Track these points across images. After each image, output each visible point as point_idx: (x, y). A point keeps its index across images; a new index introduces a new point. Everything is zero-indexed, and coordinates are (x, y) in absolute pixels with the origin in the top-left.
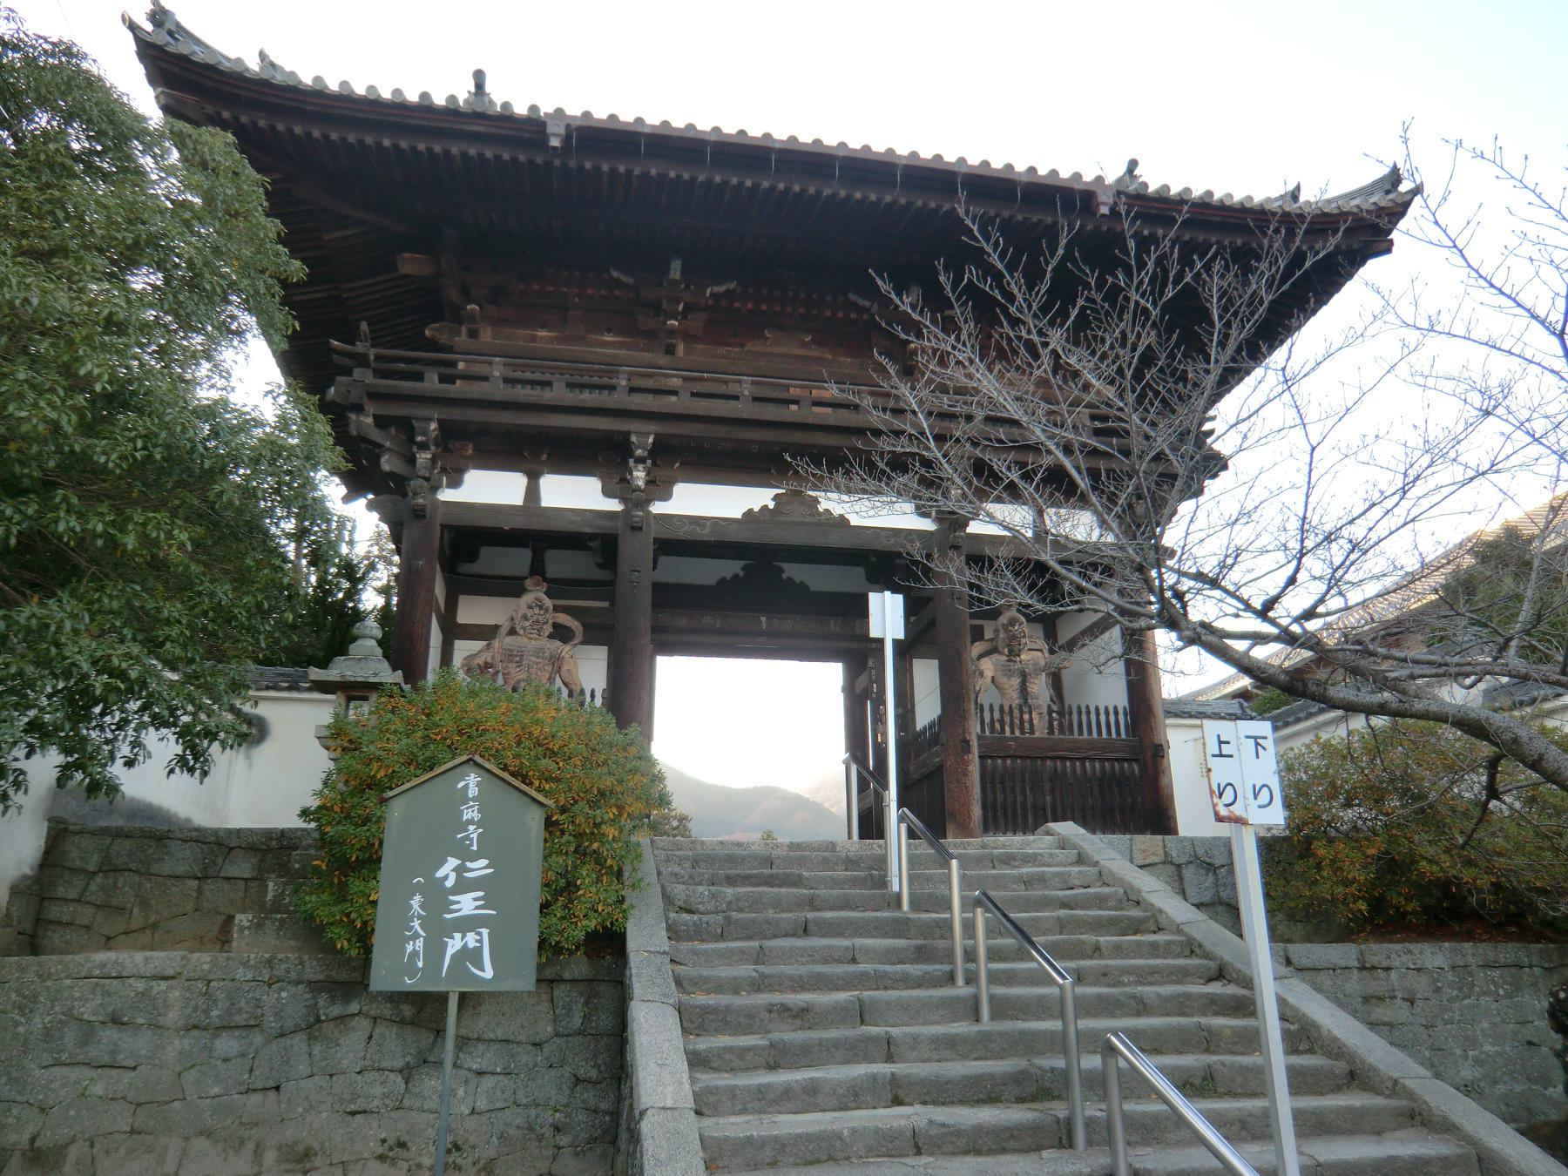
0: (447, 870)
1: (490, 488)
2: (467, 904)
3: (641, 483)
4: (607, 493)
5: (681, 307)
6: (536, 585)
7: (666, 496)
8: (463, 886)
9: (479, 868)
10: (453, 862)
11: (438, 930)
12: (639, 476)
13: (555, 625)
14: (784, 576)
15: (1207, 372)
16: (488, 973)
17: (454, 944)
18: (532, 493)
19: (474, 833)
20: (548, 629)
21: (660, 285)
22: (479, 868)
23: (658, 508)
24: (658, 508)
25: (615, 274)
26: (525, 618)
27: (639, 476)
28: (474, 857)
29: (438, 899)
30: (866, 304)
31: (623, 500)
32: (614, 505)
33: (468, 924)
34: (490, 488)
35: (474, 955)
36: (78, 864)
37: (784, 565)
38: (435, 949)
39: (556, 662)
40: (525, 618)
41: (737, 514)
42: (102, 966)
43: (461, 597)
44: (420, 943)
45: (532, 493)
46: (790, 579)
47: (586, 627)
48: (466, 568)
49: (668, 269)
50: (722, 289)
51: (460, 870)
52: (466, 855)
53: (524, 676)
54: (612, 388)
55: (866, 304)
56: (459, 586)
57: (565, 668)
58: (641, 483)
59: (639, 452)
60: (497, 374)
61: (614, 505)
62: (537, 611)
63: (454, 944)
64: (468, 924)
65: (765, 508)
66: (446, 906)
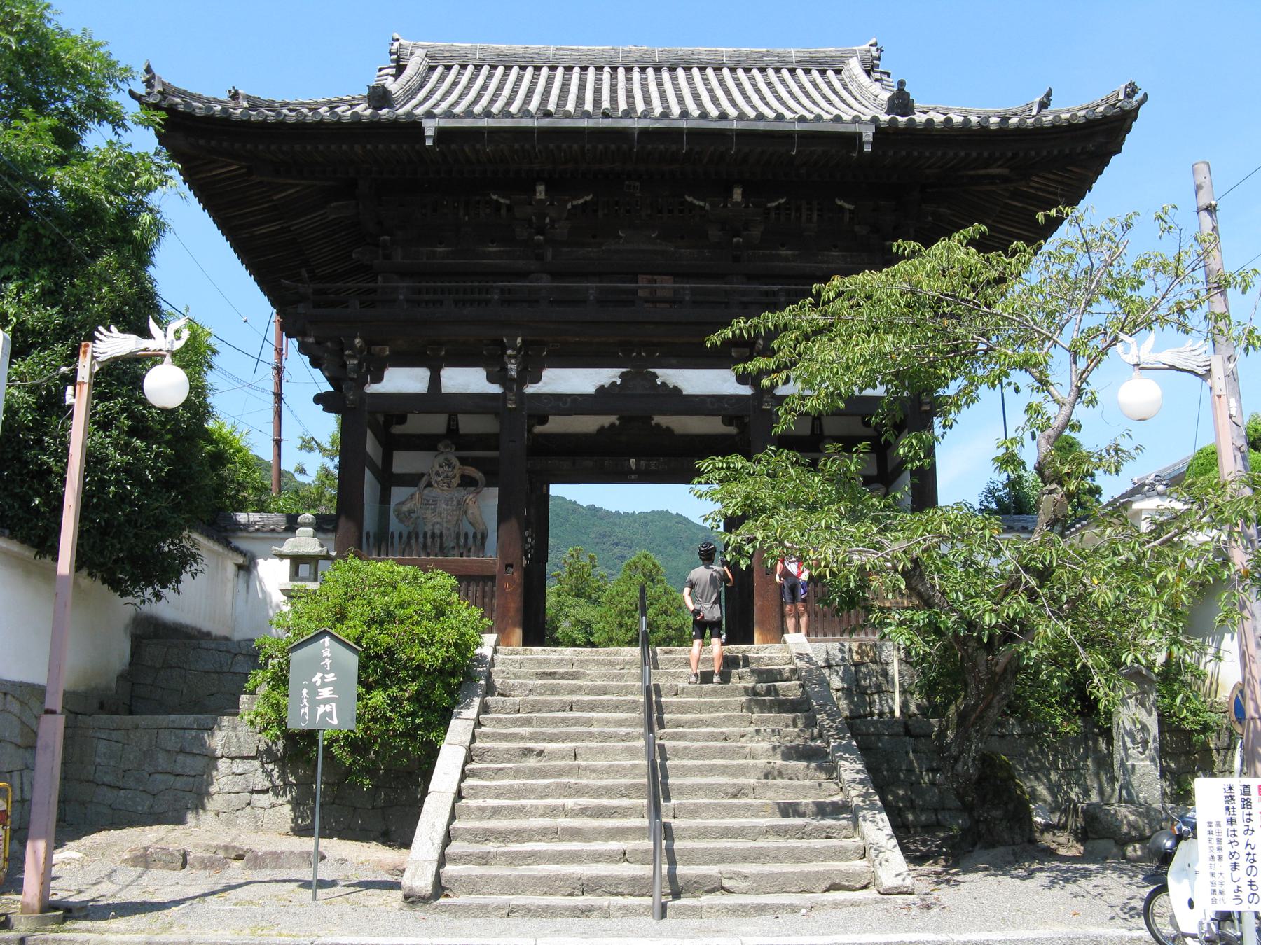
0: (317, 678)
1: (403, 380)
2: (326, 693)
3: (514, 373)
4: (491, 379)
5: (547, 220)
6: (446, 447)
7: (537, 379)
8: (324, 685)
9: (331, 677)
10: (319, 675)
11: (314, 704)
12: (513, 368)
13: (463, 476)
14: (653, 423)
15: (461, 555)
16: (335, 722)
17: (321, 709)
18: (435, 381)
19: (328, 662)
20: (457, 481)
21: (530, 204)
22: (331, 677)
23: (530, 389)
24: (530, 389)
25: (495, 197)
26: (438, 474)
27: (513, 368)
28: (328, 672)
29: (313, 690)
30: (702, 204)
31: (502, 384)
32: (496, 389)
33: (326, 701)
34: (403, 380)
35: (330, 715)
36: (149, 663)
37: (658, 371)
38: (313, 711)
39: (461, 505)
40: (438, 474)
41: (591, 390)
42: (173, 722)
43: (396, 454)
44: (306, 710)
45: (435, 381)
46: (664, 384)
47: (485, 474)
48: (397, 429)
49: (534, 191)
50: (580, 201)
51: (322, 678)
52: (325, 672)
53: (439, 520)
54: (487, 302)
55: (702, 204)
56: (391, 444)
57: (470, 511)
58: (514, 373)
59: (509, 352)
60: (401, 297)
61: (496, 389)
62: (446, 468)
63: (321, 709)
64: (326, 701)
65: (614, 383)
66: (317, 694)
